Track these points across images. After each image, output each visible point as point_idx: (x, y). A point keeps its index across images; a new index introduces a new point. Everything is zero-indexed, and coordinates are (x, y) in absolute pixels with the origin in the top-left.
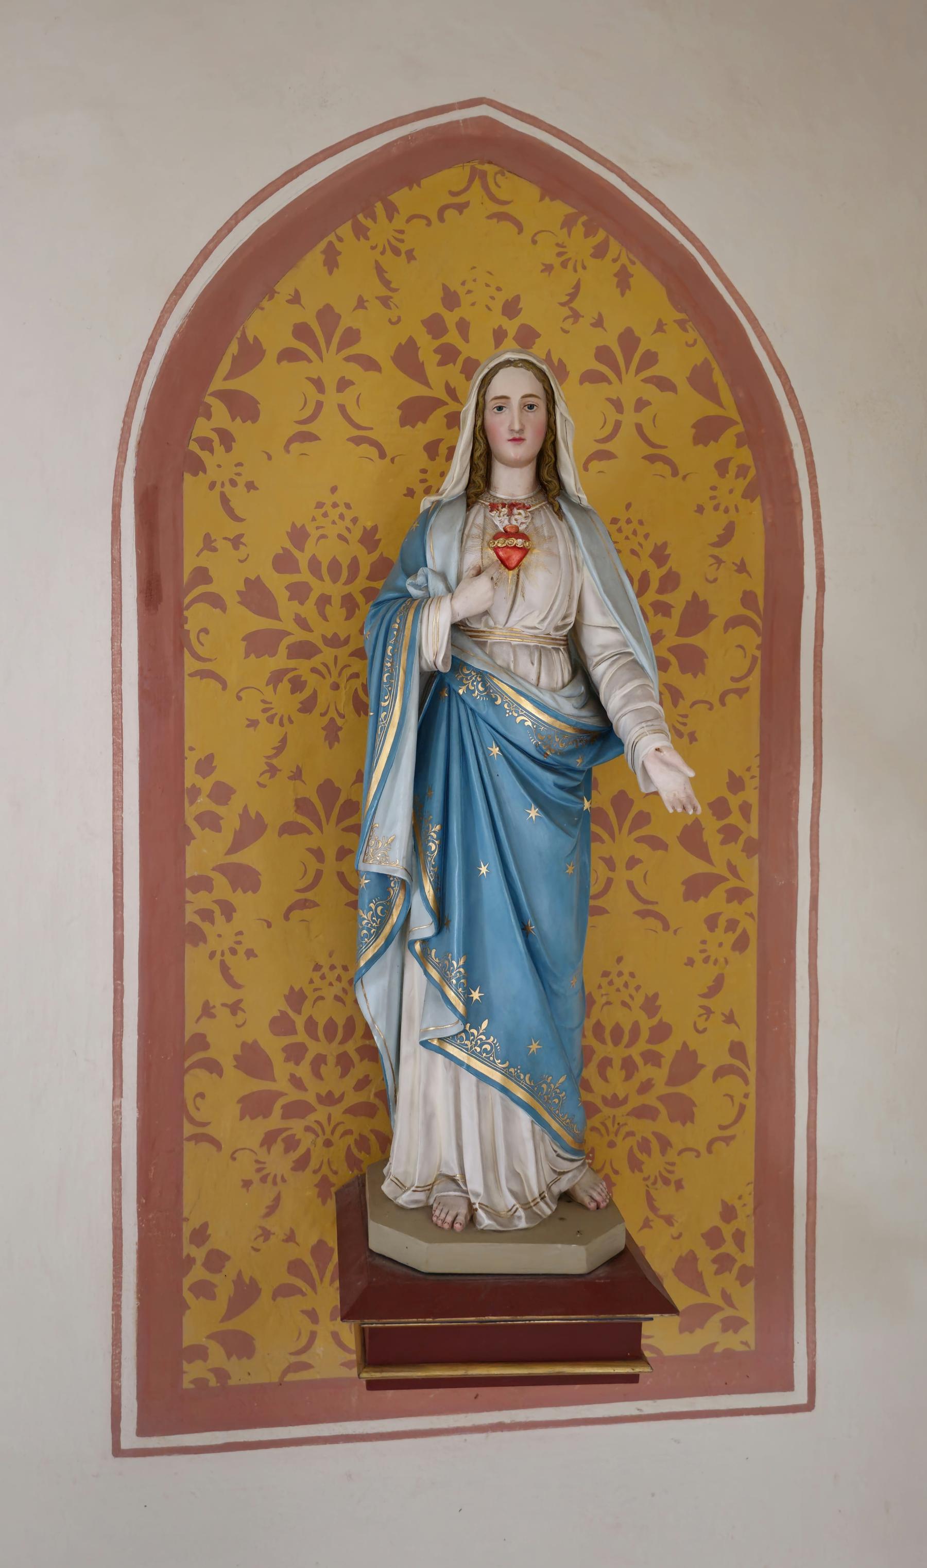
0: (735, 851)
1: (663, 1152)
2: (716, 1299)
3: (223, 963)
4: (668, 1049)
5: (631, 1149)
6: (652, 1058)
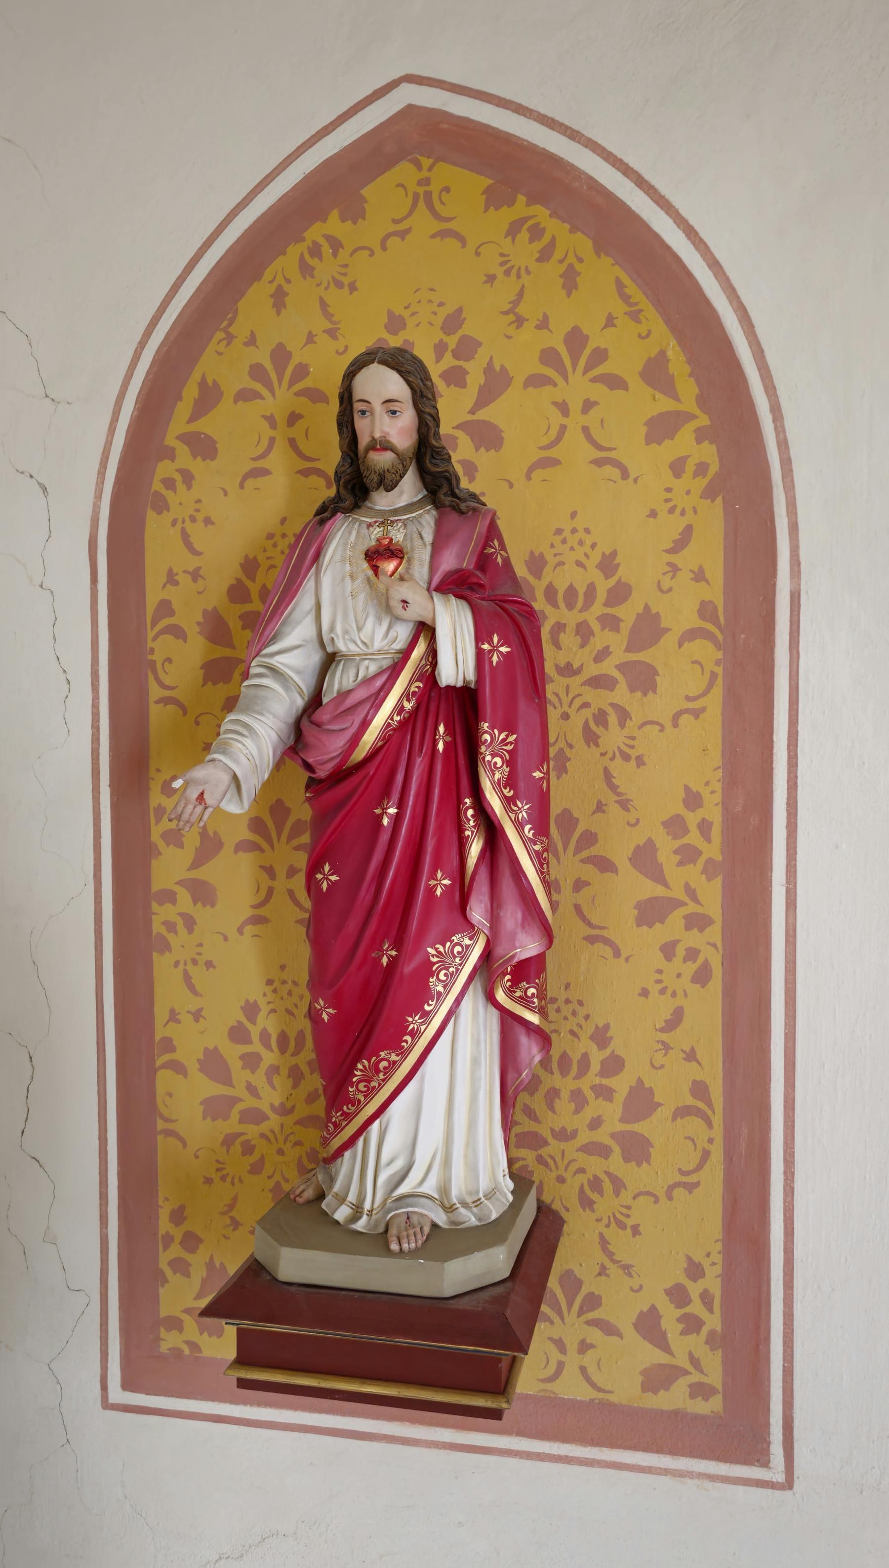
0: (693, 873)
1: (622, 724)
2: (678, 893)
3: (183, 531)
4: (628, 613)
5: (586, 722)
6: (611, 623)
